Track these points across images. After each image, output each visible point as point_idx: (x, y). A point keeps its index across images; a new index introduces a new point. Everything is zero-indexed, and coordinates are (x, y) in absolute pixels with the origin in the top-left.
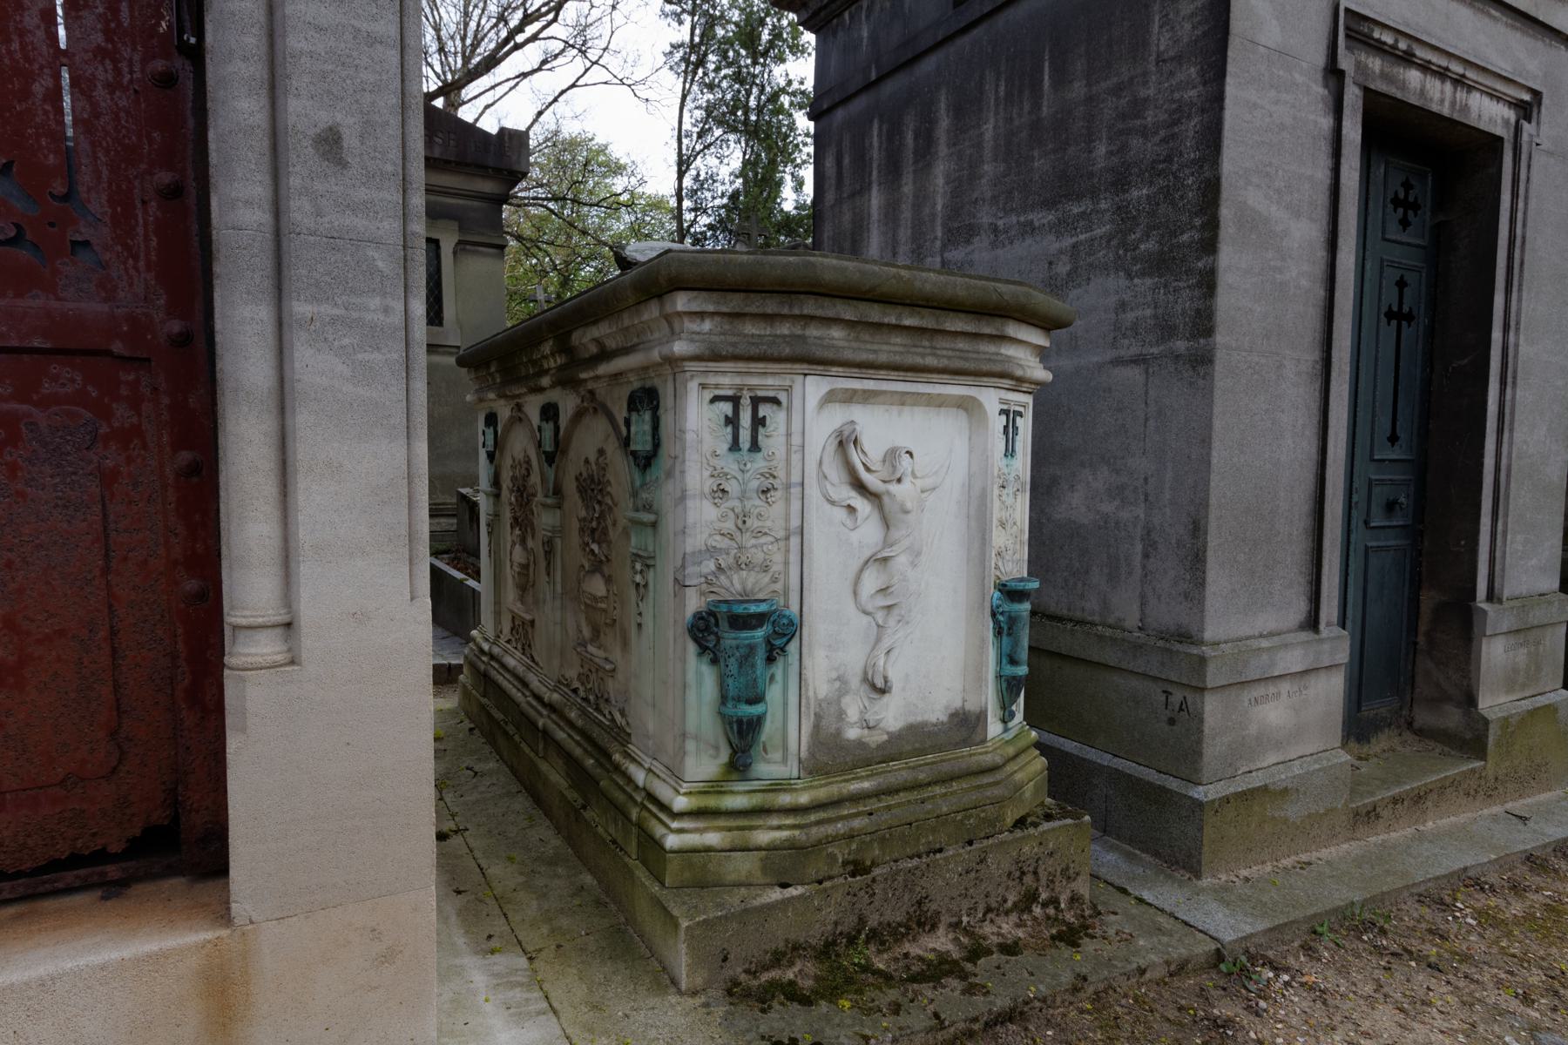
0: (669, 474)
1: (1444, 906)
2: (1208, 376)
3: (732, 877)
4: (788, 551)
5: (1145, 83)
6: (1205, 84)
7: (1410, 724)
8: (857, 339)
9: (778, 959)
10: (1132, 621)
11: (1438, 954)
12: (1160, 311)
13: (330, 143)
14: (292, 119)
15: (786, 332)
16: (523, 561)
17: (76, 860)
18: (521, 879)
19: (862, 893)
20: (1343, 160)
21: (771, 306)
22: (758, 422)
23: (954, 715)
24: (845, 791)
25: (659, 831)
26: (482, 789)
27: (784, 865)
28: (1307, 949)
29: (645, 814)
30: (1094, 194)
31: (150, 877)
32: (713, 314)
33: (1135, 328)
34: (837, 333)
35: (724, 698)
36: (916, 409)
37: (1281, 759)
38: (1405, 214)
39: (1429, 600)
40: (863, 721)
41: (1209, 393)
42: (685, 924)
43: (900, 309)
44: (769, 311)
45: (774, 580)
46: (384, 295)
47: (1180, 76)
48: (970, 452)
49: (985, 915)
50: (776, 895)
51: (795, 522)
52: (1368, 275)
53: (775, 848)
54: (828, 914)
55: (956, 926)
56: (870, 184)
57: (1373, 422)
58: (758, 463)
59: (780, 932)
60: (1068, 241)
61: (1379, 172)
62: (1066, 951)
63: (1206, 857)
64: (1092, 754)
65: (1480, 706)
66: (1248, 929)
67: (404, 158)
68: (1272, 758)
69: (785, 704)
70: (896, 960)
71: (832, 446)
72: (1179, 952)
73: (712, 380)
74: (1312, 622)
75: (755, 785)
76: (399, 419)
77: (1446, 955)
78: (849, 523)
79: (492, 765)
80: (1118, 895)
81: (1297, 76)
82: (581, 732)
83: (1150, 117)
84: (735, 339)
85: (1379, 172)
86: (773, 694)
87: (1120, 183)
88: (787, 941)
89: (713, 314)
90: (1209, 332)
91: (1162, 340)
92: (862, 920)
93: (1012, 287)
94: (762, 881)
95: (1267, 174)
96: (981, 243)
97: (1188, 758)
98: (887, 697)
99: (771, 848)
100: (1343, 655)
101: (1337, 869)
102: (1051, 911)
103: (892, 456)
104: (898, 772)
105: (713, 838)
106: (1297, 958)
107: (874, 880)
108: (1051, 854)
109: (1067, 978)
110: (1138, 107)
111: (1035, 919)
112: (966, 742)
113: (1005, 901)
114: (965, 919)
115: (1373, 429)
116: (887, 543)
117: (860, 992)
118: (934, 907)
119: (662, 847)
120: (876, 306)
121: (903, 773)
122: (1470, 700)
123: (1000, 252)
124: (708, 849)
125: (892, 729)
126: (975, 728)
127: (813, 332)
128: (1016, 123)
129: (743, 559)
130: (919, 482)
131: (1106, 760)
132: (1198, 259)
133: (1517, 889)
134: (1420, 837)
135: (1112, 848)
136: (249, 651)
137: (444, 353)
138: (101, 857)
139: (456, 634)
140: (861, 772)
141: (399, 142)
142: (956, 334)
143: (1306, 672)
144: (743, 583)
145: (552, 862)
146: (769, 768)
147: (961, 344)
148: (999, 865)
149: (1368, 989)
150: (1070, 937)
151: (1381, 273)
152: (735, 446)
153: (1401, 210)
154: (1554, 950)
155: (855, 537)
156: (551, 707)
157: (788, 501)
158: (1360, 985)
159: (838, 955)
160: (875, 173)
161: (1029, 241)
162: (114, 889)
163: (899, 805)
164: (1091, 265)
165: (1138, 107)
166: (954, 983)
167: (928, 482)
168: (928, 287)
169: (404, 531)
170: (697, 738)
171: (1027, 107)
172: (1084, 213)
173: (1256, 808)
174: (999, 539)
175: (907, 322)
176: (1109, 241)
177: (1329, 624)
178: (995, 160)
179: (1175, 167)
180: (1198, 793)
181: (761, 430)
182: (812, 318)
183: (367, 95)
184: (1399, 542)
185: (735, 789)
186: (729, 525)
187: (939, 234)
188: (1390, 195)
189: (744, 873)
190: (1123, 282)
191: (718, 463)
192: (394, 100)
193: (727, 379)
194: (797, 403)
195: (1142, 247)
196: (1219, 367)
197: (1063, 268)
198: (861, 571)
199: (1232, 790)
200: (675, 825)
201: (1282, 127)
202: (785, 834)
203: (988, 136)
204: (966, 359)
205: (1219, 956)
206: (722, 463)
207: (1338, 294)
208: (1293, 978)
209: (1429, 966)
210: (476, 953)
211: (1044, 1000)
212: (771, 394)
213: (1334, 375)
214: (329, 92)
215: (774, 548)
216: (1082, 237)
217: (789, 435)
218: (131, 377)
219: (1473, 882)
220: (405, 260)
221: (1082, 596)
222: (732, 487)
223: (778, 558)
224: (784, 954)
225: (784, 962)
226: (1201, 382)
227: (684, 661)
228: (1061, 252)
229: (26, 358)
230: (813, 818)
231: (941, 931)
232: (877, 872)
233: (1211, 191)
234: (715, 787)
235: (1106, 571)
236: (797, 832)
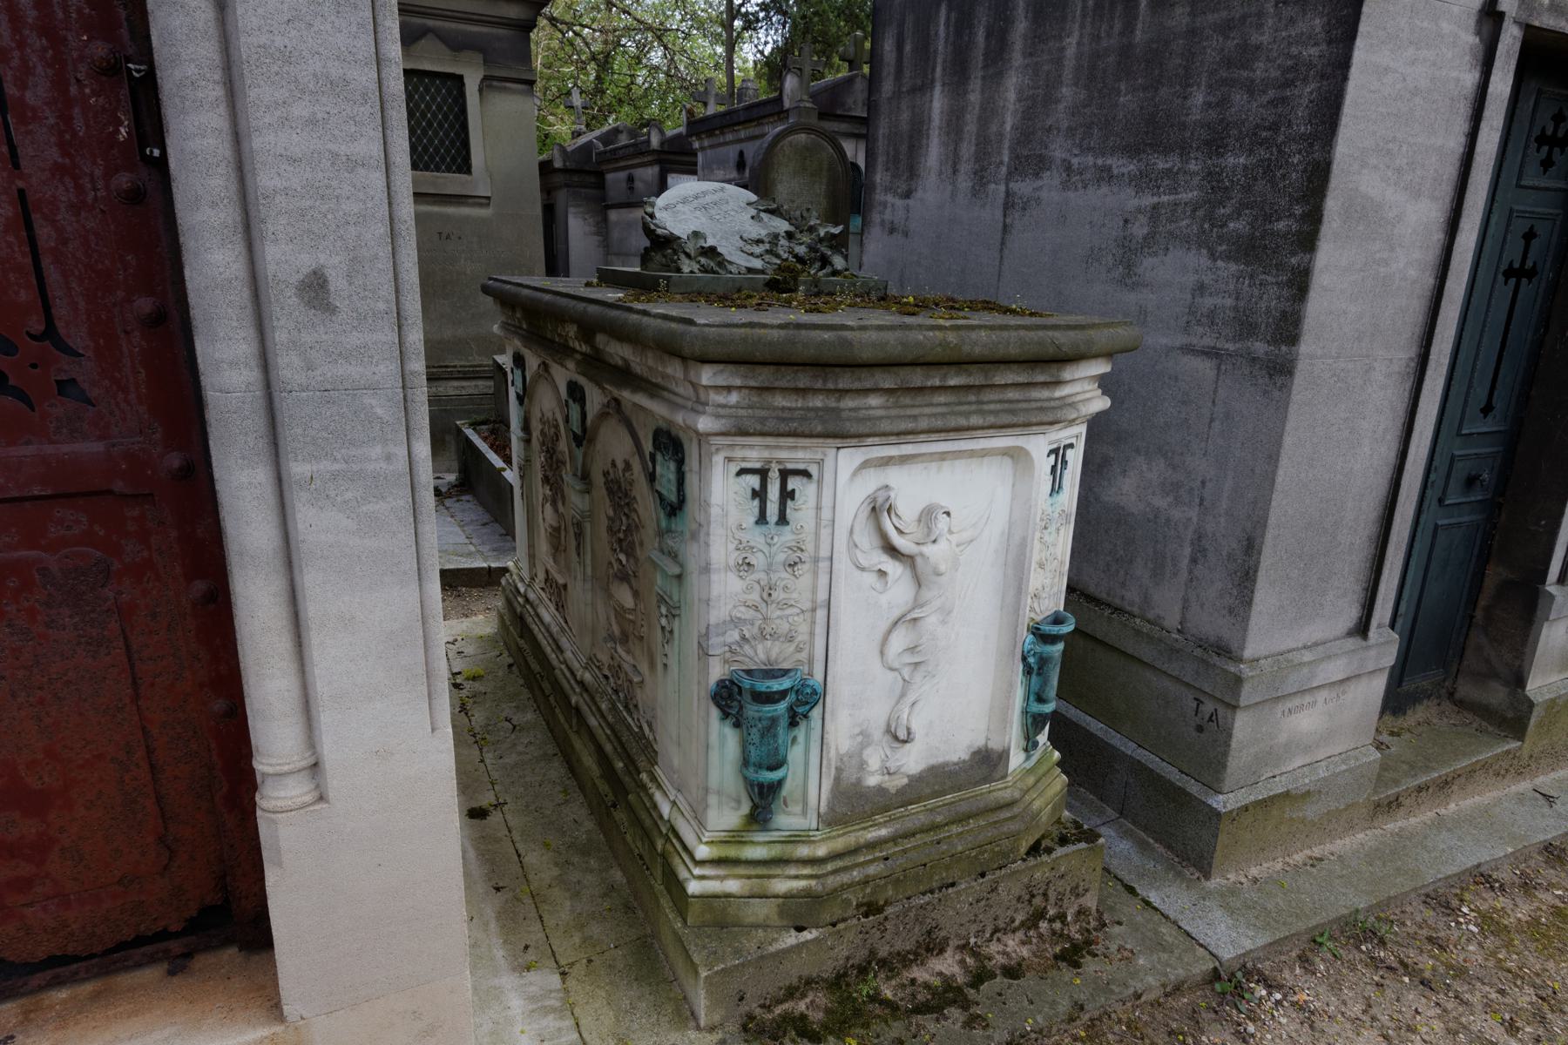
0: (694, 536)
1: (1450, 910)
2: (1286, 388)
4: (813, 623)
5: (1260, 26)
6: (1329, 43)
7: (1451, 695)
8: (897, 406)
9: (791, 993)
11: (1434, 969)
13: (315, 288)
14: (271, 269)
16: (555, 524)
17: (140, 941)
18: (556, 872)
20: (1483, 125)
21: (803, 381)
22: (787, 495)
23: (975, 754)
24: (862, 841)
25: (683, 873)
26: (520, 748)
27: (799, 911)
28: (1304, 960)
29: (668, 846)
30: (1184, 150)
31: (208, 948)
32: (740, 388)
33: (1212, 315)
35: (745, 762)
37: (1308, 761)
38: (1550, 153)
39: (1495, 575)
40: (882, 768)
41: (1282, 409)
42: (704, 974)
44: (801, 385)
47: (1302, 27)
50: (791, 939)
51: (822, 596)
52: (1491, 231)
53: (792, 896)
55: (962, 948)
56: (933, 81)
57: (1468, 393)
58: (786, 536)
59: (793, 972)
60: (1148, 200)
61: (1527, 105)
62: (1067, 973)
63: (1216, 862)
64: (1115, 739)
65: (1528, 687)
66: (1248, 945)
67: (397, 291)
68: (1298, 762)
69: (807, 764)
70: (903, 986)
71: (866, 509)
72: (1177, 973)
74: (1362, 629)
75: (774, 836)
77: (1441, 969)
78: (878, 586)
79: (530, 716)
80: (1125, 895)
81: (1444, 25)
82: (613, 730)
83: (1260, 70)
84: (763, 413)
85: (1527, 105)
86: (795, 755)
87: (1215, 144)
88: (800, 978)
89: (740, 388)
90: (1293, 339)
91: (1239, 337)
92: (873, 952)
93: (1072, 334)
94: (778, 923)
95: (1389, 152)
96: (1052, 179)
97: (1212, 767)
99: (788, 896)
100: (1389, 658)
101: (1343, 865)
102: (1057, 925)
103: (928, 516)
104: (917, 814)
105: (733, 886)
106: (1292, 970)
107: (886, 918)
108: (1062, 876)
109: (1064, 1006)
110: (1247, 54)
111: (1040, 936)
112: (986, 779)
113: (1013, 921)
114: (972, 940)
115: (1466, 401)
116: (917, 604)
117: (866, 1026)
118: (943, 934)
119: (684, 890)
120: (918, 369)
121: (921, 817)
122: (1519, 681)
123: (1071, 194)
124: (728, 896)
126: (995, 766)
128: (1104, 43)
129: (768, 630)
130: (954, 538)
131: (1129, 748)
132: (1293, 254)
133: (1527, 886)
134: (1440, 823)
135: (1126, 834)
136: (281, 802)
137: (468, 205)
138: (163, 935)
139: (496, 521)
140: (879, 818)
141: (391, 275)
143: (1342, 681)
144: (767, 653)
145: (585, 850)
146: (788, 820)
147: (1012, 394)
148: (1009, 890)
149: (1356, 1009)
150: (1072, 956)
151: (1508, 225)
152: (762, 519)
153: (1545, 149)
154: (1551, 965)
155: (884, 599)
156: (581, 683)
157: (815, 574)
158: (1350, 1003)
159: (848, 985)
160: (939, 69)
161: (1104, 189)
162: (178, 965)
164: (1171, 233)
165: (1247, 54)
166: (954, 1013)
167: (966, 535)
169: (421, 670)
170: (719, 793)
171: (1118, 26)
172: (1170, 170)
173: (1275, 812)
174: (1036, 580)
175: (952, 383)
176: (1194, 210)
177: (1379, 626)
178: (1076, 84)
179: (1281, 139)
182: (847, 391)
183: (352, 229)
184: (1473, 517)
187: (1006, 159)
188: (1536, 132)
190: (1205, 261)
191: (744, 537)
192: (382, 229)
193: (754, 453)
194: (828, 477)
195: (1232, 225)
196: (1299, 379)
197: (1139, 230)
198: (889, 632)
199: (1252, 798)
200: (697, 871)
201: (1416, 92)
202: (802, 884)
203: (1071, 52)
205: (1215, 975)
206: (748, 537)
207: (1448, 284)
208: (1285, 996)
209: (1422, 983)
210: (514, 970)
211: (1041, 1032)
212: (801, 466)
213: (1429, 373)
214: (310, 231)
216: (1165, 198)
217: (818, 508)
218: (136, 513)
219: (1483, 878)
220: (405, 400)
221: (1123, 585)
222: (758, 560)
223: (804, 628)
226: (1276, 393)
227: (707, 724)
228: (1139, 210)
229: (27, 505)
230: (830, 867)
231: (949, 952)
232: (889, 910)
233: (1318, 177)
234: (735, 838)
235: (1150, 565)
236: (813, 882)
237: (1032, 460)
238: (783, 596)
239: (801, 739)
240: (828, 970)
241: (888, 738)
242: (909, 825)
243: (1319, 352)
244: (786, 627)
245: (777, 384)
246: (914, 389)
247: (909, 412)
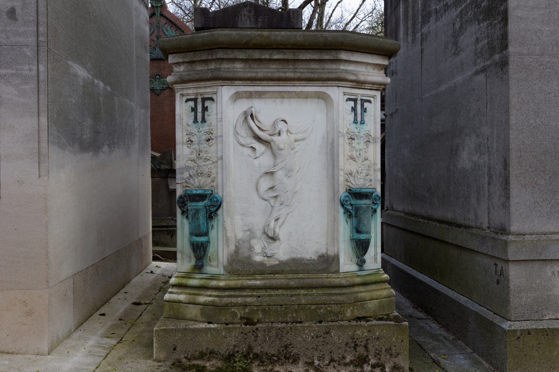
2: (506, 73)
3: (189, 316)
8: (250, 67)
9: (202, 356)
10: (485, 225)
12: (490, 39)
15: (213, 67)
19: (250, 334)
21: (204, 56)
22: (205, 109)
23: (321, 257)
27: (211, 312)
32: (183, 63)
34: (238, 66)
36: (292, 100)
43: (271, 51)
44: (203, 58)
45: (213, 181)
46: (29, 64)
48: (327, 120)
49: (330, 362)
54: (231, 340)
58: (205, 128)
73: (185, 92)
76: (35, 110)
78: (252, 155)
86: (213, 234)
88: (207, 348)
89: (183, 63)
92: (250, 348)
94: (201, 320)
98: (277, 243)
99: (205, 304)
104: (279, 280)
105: (182, 297)
112: (325, 271)
114: (316, 362)
120: (257, 51)
121: (282, 281)
124: (180, 302)
127: (225, 66)
129: (199, 171)
132: (501, 5)
142: (307, 60)
144: (199, 182)
146: (210, 269)
152: (195, 121)
155: (256, 162)
163: (277, 295)
167: (299, 136)
168: (279, 38)
169: (36, 151)
175: (276, 57)
180: (506, 325)
181: (206, 113)
185: (196, 277)
186: (194, 156)
189: (194, 315)
191: (189, 129)
193: (191, 90)
199: (534, 327)
204: (312, 73)
212: (210, 96)
215: (213, 166)
220: (38, 50)
224: (206, 354)
225: (206, 358)
231: (301, 364)
232: (259, 325)
234: (188, 275)
236: (216, 299)
237: (332, 99)
238: (205, 155)
239: (215, 226)
240: (223, 350)
242: (274, 282)
243: (526, 52)
244: (207, 170)
245: (195, 59)
246: (255, 59)
247: (255, 70)
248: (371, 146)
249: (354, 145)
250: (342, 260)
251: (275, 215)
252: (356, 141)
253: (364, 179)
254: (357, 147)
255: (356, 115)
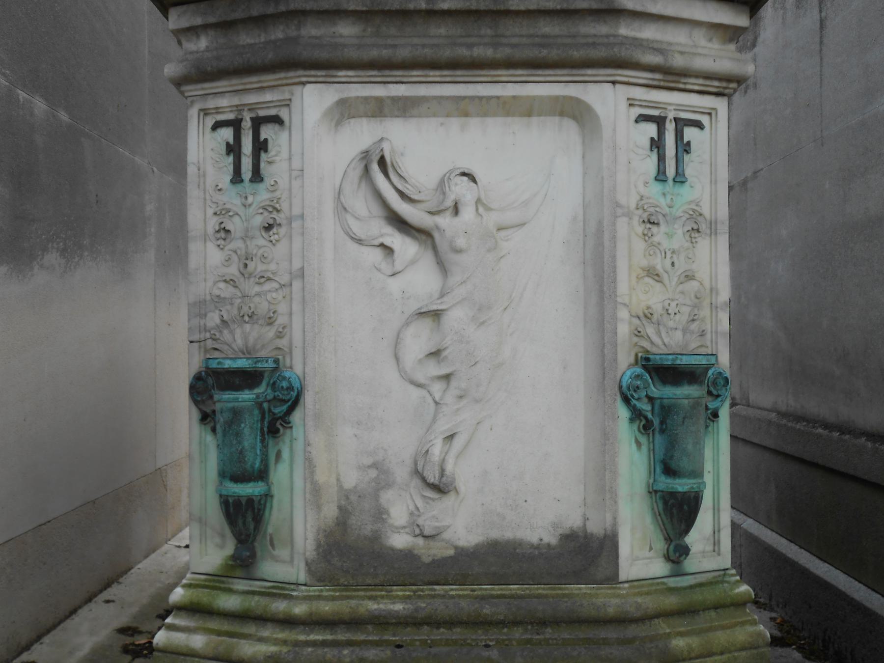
22: (260, 146)
24: (362, 610)
32: (206, 27)
36: (489, 120)
44: (255, 13)
45: (280, 335)
48: (585, 174)
58: (261, 195)
73: (211, 103)
75: (256, 585)
78: (385, 267)
86: (279, 474)
89: (206, 27)
98: (449, 501)
104: (455, 597)
112: (578, 577)
125: (462, 543)
129: (245, 309)
140: (398, 591)
144: (245, 338)
152: (237, 178)
155: (394, 285)
181: (263, 156)
186: (233, 271)
191: (222, 198)
212: (272, 112)
215: (279, 295)
222: (235, 225)
234: (217, 581)
236: (285, 649)
238: (261, 267)
239: (285, 454)
241: (416, 482)
242: (440, 608)
248: (703, 244)
249: (656, 239)
250: (625, 548)
251: (443, 426)
252: (663, 228)
253: (685, 331)
254: (666, 244)
255: (661, 159)
